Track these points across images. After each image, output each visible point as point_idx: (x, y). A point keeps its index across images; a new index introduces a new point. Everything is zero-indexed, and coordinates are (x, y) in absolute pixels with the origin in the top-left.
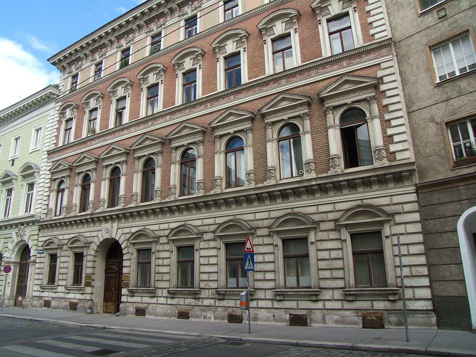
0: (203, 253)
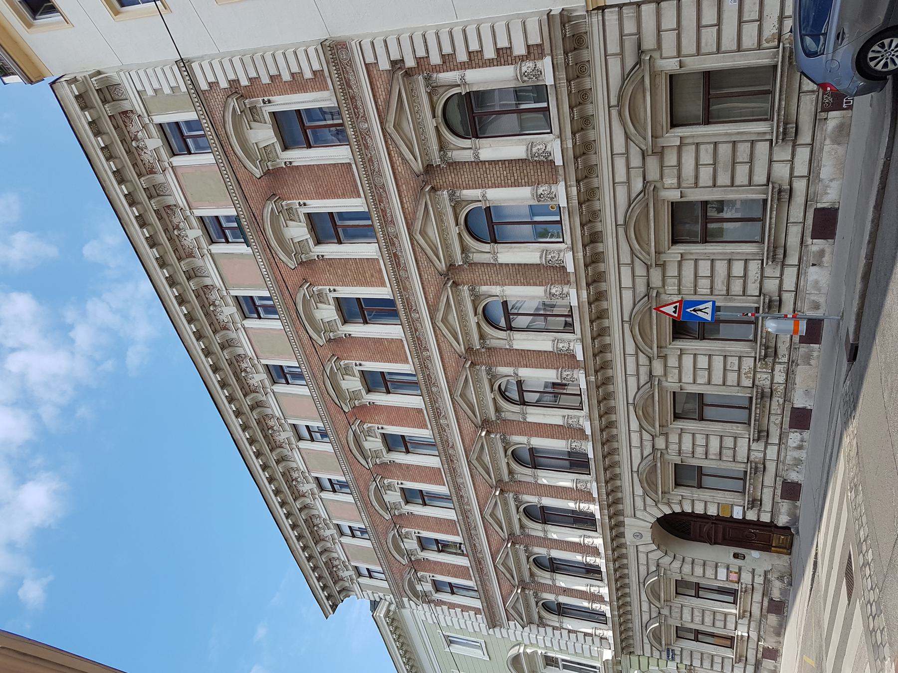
0: (687, 378)
